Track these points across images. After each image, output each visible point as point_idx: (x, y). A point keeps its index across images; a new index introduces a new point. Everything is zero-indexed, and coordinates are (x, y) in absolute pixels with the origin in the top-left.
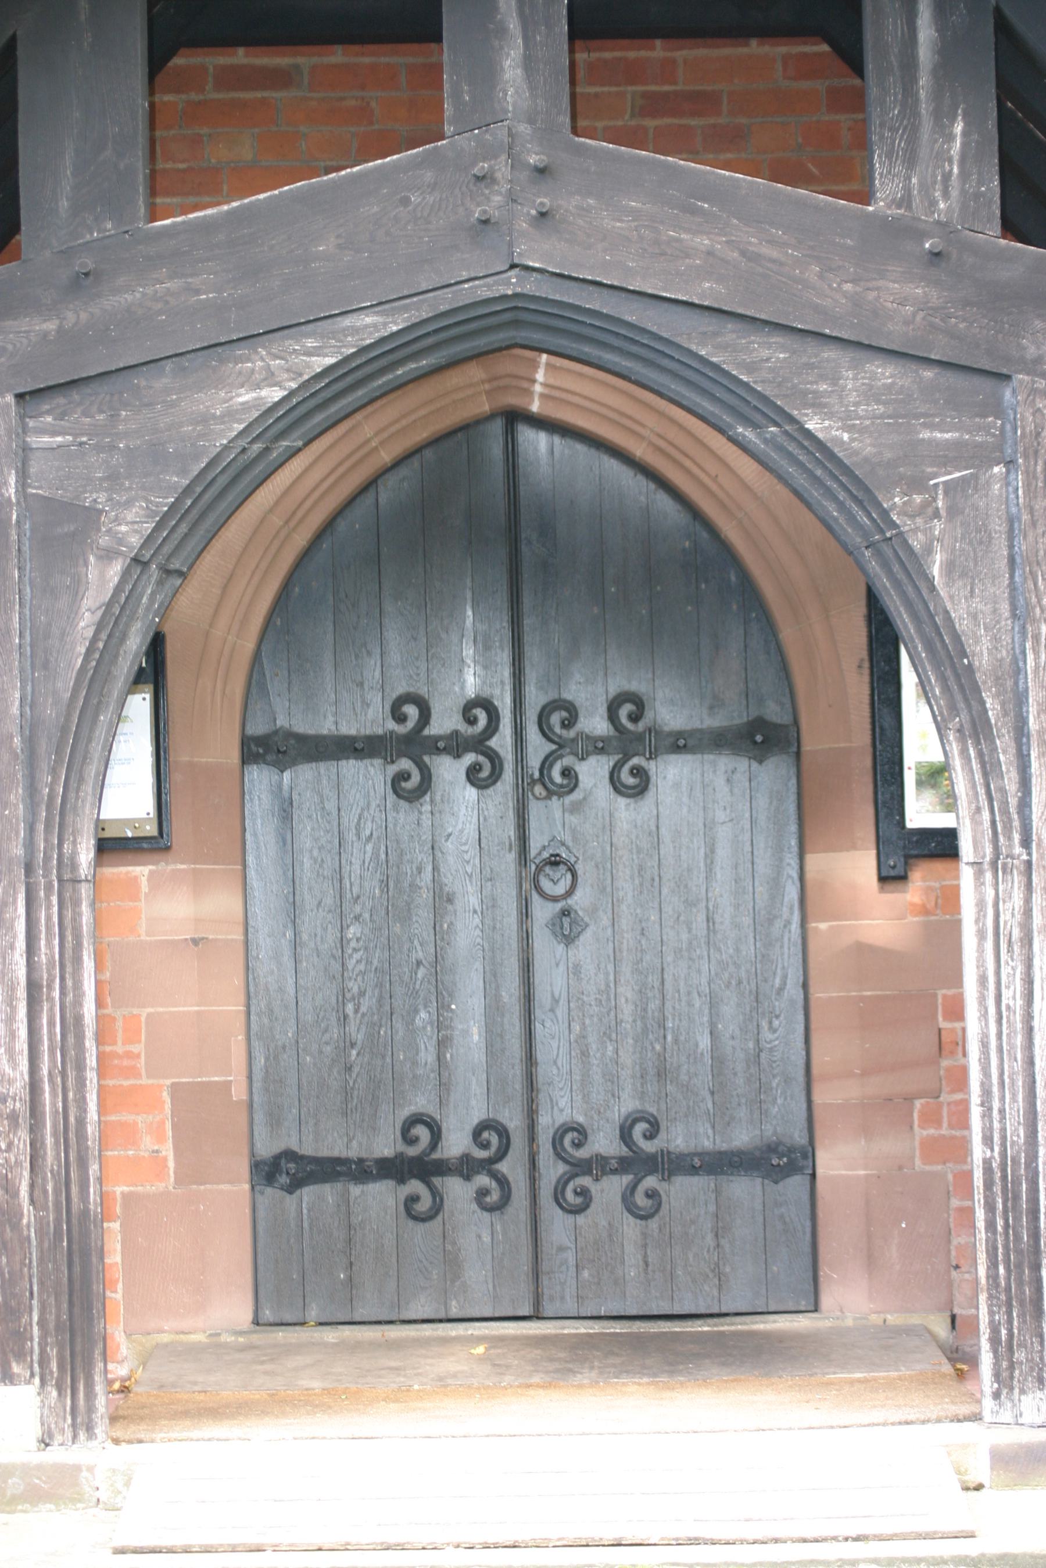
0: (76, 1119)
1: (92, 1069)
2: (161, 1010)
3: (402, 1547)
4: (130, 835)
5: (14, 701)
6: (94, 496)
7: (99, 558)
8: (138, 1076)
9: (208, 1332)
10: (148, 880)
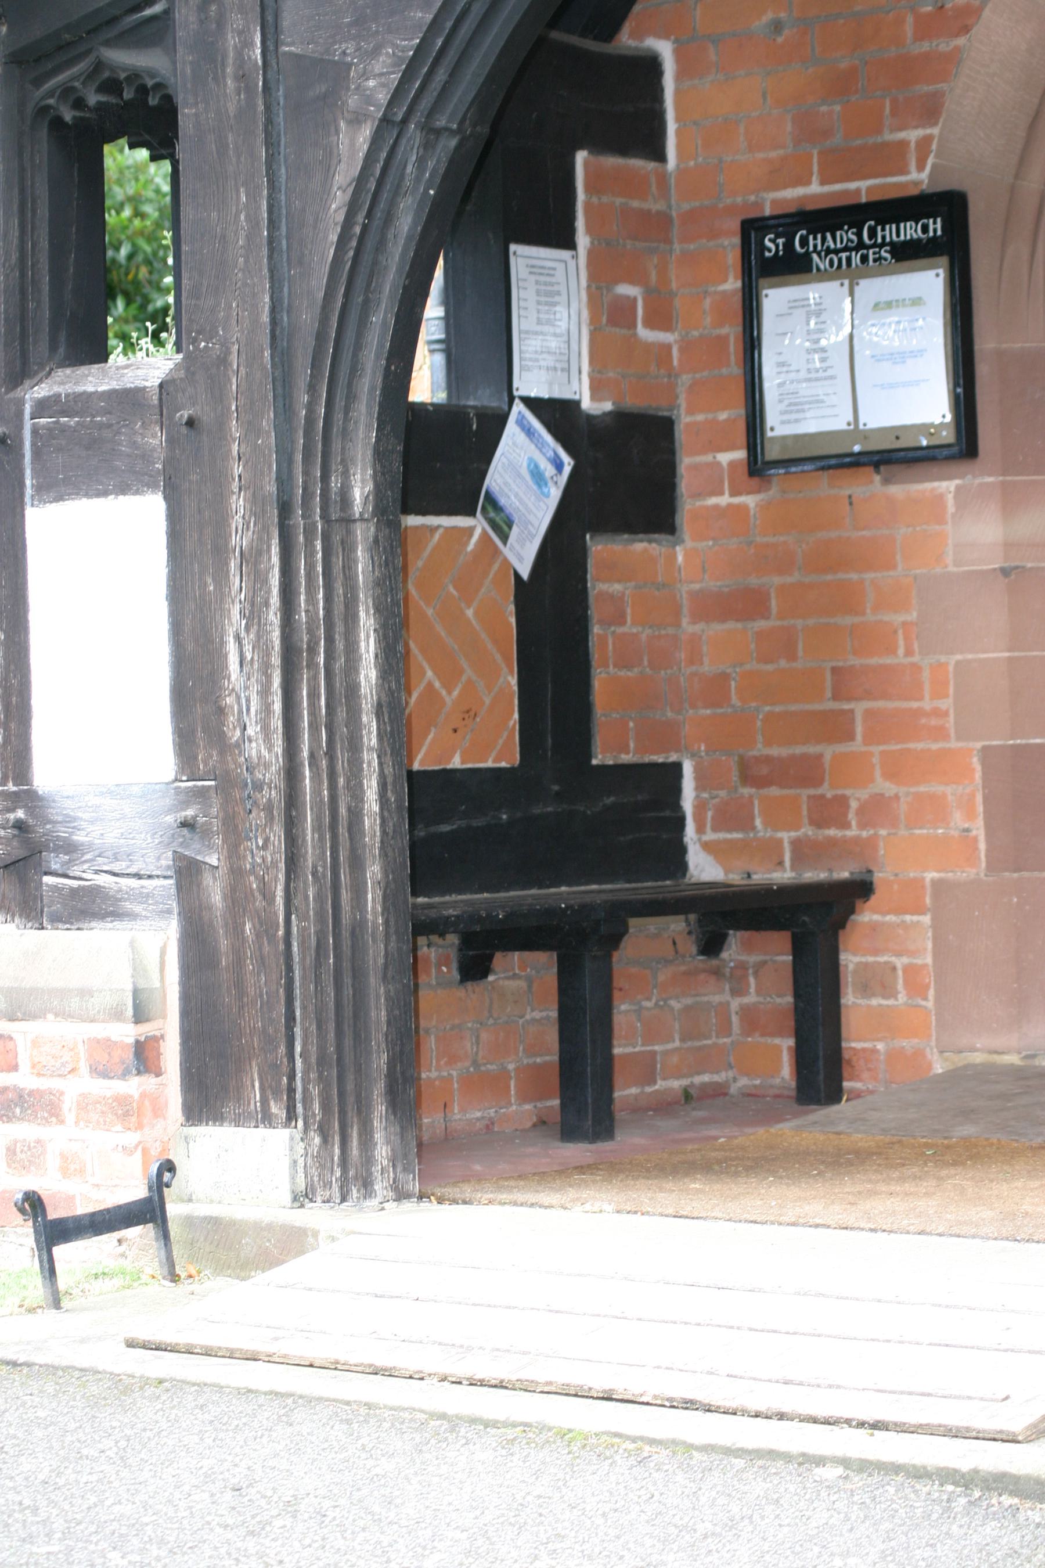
0: (349, 809)
1: (370, 749)
2: (970, 656)
3: (388, 1373)
4: (924, 443)
5: (264, 306)
6: (344, 46)
7: (349, 122)
8: (946, 737)
9: (1024, 1053)
10: (955, 497)
